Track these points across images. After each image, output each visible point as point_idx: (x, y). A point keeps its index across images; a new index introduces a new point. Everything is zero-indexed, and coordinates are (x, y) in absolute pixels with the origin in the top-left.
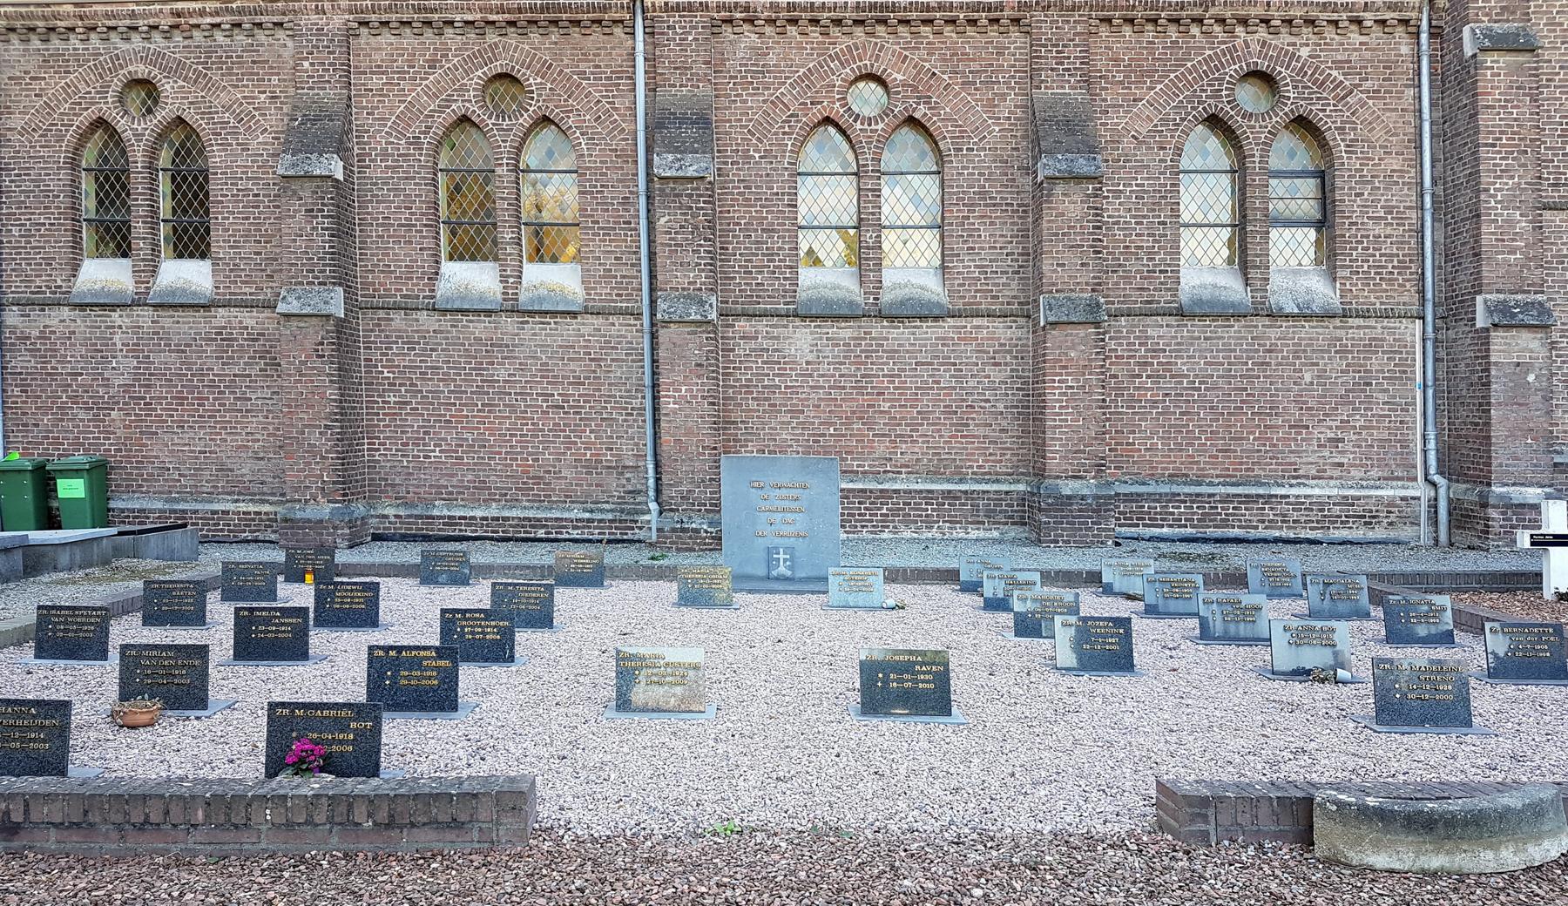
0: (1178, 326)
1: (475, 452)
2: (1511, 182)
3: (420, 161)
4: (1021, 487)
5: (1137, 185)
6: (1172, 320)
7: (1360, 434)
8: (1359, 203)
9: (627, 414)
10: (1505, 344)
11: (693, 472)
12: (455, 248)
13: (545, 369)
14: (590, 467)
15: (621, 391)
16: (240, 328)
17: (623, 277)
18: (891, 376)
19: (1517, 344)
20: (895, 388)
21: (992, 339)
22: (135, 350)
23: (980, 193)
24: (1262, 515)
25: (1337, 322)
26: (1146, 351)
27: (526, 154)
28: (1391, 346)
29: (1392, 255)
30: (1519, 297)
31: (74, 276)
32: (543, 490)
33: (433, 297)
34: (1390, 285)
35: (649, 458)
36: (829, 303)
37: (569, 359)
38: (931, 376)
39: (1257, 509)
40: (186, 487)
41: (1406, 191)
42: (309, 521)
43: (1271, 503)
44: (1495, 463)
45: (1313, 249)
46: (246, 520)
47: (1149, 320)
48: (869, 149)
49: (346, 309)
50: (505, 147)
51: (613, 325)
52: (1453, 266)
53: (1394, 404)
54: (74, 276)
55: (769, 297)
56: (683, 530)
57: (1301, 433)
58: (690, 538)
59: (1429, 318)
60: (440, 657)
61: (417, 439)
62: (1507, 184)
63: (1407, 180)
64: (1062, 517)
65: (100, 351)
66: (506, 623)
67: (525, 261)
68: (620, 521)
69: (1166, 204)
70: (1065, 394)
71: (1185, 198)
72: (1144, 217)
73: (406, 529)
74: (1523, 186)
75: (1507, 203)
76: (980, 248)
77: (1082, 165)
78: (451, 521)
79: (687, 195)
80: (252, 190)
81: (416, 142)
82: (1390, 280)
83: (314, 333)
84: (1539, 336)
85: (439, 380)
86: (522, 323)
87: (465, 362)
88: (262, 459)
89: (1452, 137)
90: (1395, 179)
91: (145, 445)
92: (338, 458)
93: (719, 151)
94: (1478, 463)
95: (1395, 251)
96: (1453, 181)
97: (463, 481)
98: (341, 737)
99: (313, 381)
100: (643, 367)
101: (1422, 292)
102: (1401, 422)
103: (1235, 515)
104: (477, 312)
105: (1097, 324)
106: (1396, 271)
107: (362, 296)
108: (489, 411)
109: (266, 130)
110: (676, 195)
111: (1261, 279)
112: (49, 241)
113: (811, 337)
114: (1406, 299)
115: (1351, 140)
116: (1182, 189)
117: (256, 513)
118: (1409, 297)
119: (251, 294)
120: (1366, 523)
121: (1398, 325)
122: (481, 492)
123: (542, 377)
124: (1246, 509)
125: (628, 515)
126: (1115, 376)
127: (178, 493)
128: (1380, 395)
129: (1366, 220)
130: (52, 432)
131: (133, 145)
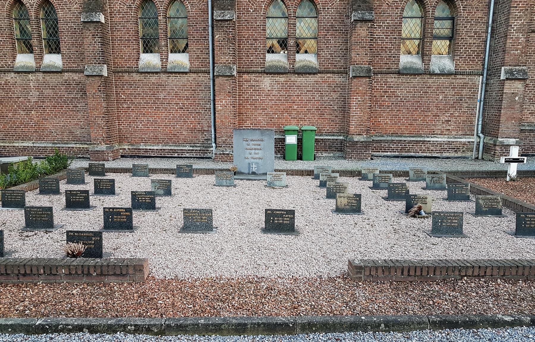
0: (398, 78)
1: (153, 125)
2: (520, 22)
3: (132, 14)
4: (341, 138)
5: (387, 23)
6: (396, 76)
7: (456, 118)
8: (465, 30)
9: (205, 111)
10: (510, 86)
11: (227, 133)
12: (145, 48)
13: (176, 94)
14: (192, 130)
15: (203, 102)
16: (73, 80)
17: (203, 58)
18: (298, 96)
19: (514, 86)
20: (299, 100)
21: (333, 82)
22: (38, 89)
23: (331, 25)
24: (421, 148)
25: (453, 77)
26: (387, 87)
27: (169, 11)
28: (471, 86)
29: (475, 51)
30: (517, 68)
31: (14, 61)
32: (177, 139)
33: (138, 67)
34: (473, 62)
35: (212, 127)
36: (276, 67)
37: (185, 90)
38: (312, 96)
39: (420, 146)
40: (59, 138)
41: (482, 26)
42: (99, 151)
43: (424, 144)
44: (500, 130)
45: (448, 48)
46: (80, 150)
47: (388, 76)
48: (292, 8)
49: (108, 73)
50: (162, 9)
51: (200, 77)
52: (496, 55)
53: (469, 107)
54: (14, 61)
55: (255, 65)
56: (223, 154)
57: (436, 118)
58: (226, 157)
59: (485, 75)
60: (126, 212)
61: (134, 120)
62: (519, 23)
63: (483, 21)
64: (354, 149)
65: (26, 88)
66: (152, 196)
67: (169, 53)
68: (203, 150)
69: (397, 31)
70: (357, 103)
71: (404, 28)
72: (389, 36)
73: (132, 153)
74: (525, 24)
75: (518, 31)
76: (331, 47)
77: (367, 16)
78: (146, 151)
79: (226, 27)
80: (73, 27)
81: (130, 7)
82: (473, 60)
83: (97, 82)
84: (522, 82)
85: (140, 99)
86: (168, 76)
87: (149, 92)
88: (83, 128)
89: (502, 4)
90: (479, 21)
91: (44, 123)
92: (108, 128)
93: (238, 9)
94: (495, 130)
95: (476, 49)
96: (500, 21)
97: (150, 136)
98: (90, 242)
99: (98, 100)
100: (210, 93)
101: (483, 65)
102: (471, 114)
103: (412, 148)
104: (153, 73)
105: (369, 77)
106: (475, 57)
107: (114, 67)
108: (158, 110)
109: (77, 3)
110: (222, 27)
111: (428, 60)
112: (4, 47)
113: (270, 81)
114: (478, 68)
115: (465, 5)
116: (403, 25)
117: (83, 148)
118: (479, 67)
119: (76, 67)
120: (455, 151)
121: (474, 78)
122: (156, 140)
123: (176, 97)
124: (416, 146)
125: (206, 148)
126: (375, 96)
127: (57, 141)
128: (465, 104)
129: (467, 37)
130: (13, 119)
131: (30, 9)
